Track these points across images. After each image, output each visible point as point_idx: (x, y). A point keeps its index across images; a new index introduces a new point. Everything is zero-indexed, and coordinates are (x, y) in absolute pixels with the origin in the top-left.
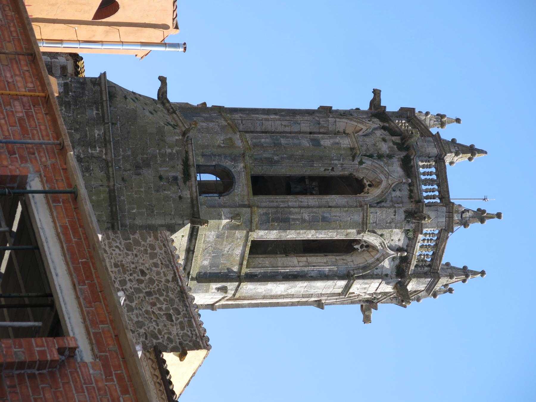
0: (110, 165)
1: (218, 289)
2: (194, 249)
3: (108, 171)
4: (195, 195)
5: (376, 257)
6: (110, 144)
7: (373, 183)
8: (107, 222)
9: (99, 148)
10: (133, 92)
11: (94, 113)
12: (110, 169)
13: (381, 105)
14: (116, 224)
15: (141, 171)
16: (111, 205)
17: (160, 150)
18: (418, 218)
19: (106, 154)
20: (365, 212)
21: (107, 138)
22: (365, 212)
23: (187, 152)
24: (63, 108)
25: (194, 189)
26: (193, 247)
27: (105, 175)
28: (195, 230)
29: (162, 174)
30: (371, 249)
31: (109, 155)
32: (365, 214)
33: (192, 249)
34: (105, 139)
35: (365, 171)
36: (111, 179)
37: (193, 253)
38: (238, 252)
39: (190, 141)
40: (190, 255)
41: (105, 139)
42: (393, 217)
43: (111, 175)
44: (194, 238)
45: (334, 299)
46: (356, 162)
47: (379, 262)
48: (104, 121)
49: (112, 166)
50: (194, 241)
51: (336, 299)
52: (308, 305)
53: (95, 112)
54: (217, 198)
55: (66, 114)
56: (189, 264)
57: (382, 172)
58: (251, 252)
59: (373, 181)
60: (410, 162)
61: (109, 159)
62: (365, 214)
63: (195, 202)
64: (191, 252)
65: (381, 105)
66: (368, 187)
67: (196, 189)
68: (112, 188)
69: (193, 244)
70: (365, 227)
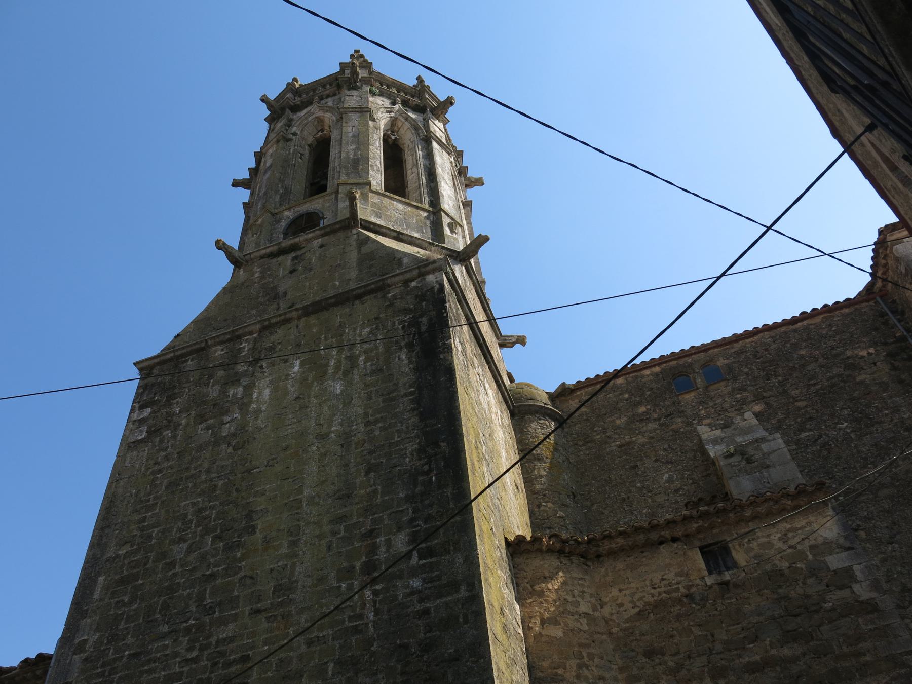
0: (266, 323)
1: (452, 231)
2: (396, 231)
3: (277, 323)
4: (318, 232)
5: (403, 120)
6: (236, 330)
7: (319, 129)
8: (353, 305)
9: (241, 344)
10: (176, 337)
11: (191, 363)
12: (274, 321)
13: (249, 178)
14: (354, 293)
15: (281, 293)
16: (326, 308)
17: (255, 283)
18: (355, 76)
19: (251, 333)
20: (347, 110)
21: (228, 337)
22: (347, 110)
23: (262, 257)
24: (175, 401)
25: (310, 235)
26: (392, 232)
27: (282, 327)
28: (367, 225)
29: (288, 272)
30: (396, 128)
31: (253, 328)
32: (350, 110)
33: (395, 234)
34: (229, 340)
35: (305, 132)
36: (288, 316)
37: (402, 234)
38: (400, 206)
39: (246, 257)
40: (405, 238)
41: (229, 340)
42: (355, 97)
43: (282, 317)
44: (378, 229)
45: (460, 192)
46: (294, 138)
47: (409, 118)
48: (203, 349)
49: (268, 319)
50: (384, 230)
51: (459, 189)
52: (472, 230)
53: (190, 363)
54: (325, 220)
55: (185, 396)
56: (418, 242)
57: (306, 118)
58: (403, 196)
59: (317, 129)
60: (298, 105)
61: (258, 326)
62: (350, 110)
63: (328, 230)
64: (401, 236)
65: (249, 178)
66: (325, 132)
67: (310, 233)
68: (301, 312)
69: (388, 232)
70: (365, 110)
